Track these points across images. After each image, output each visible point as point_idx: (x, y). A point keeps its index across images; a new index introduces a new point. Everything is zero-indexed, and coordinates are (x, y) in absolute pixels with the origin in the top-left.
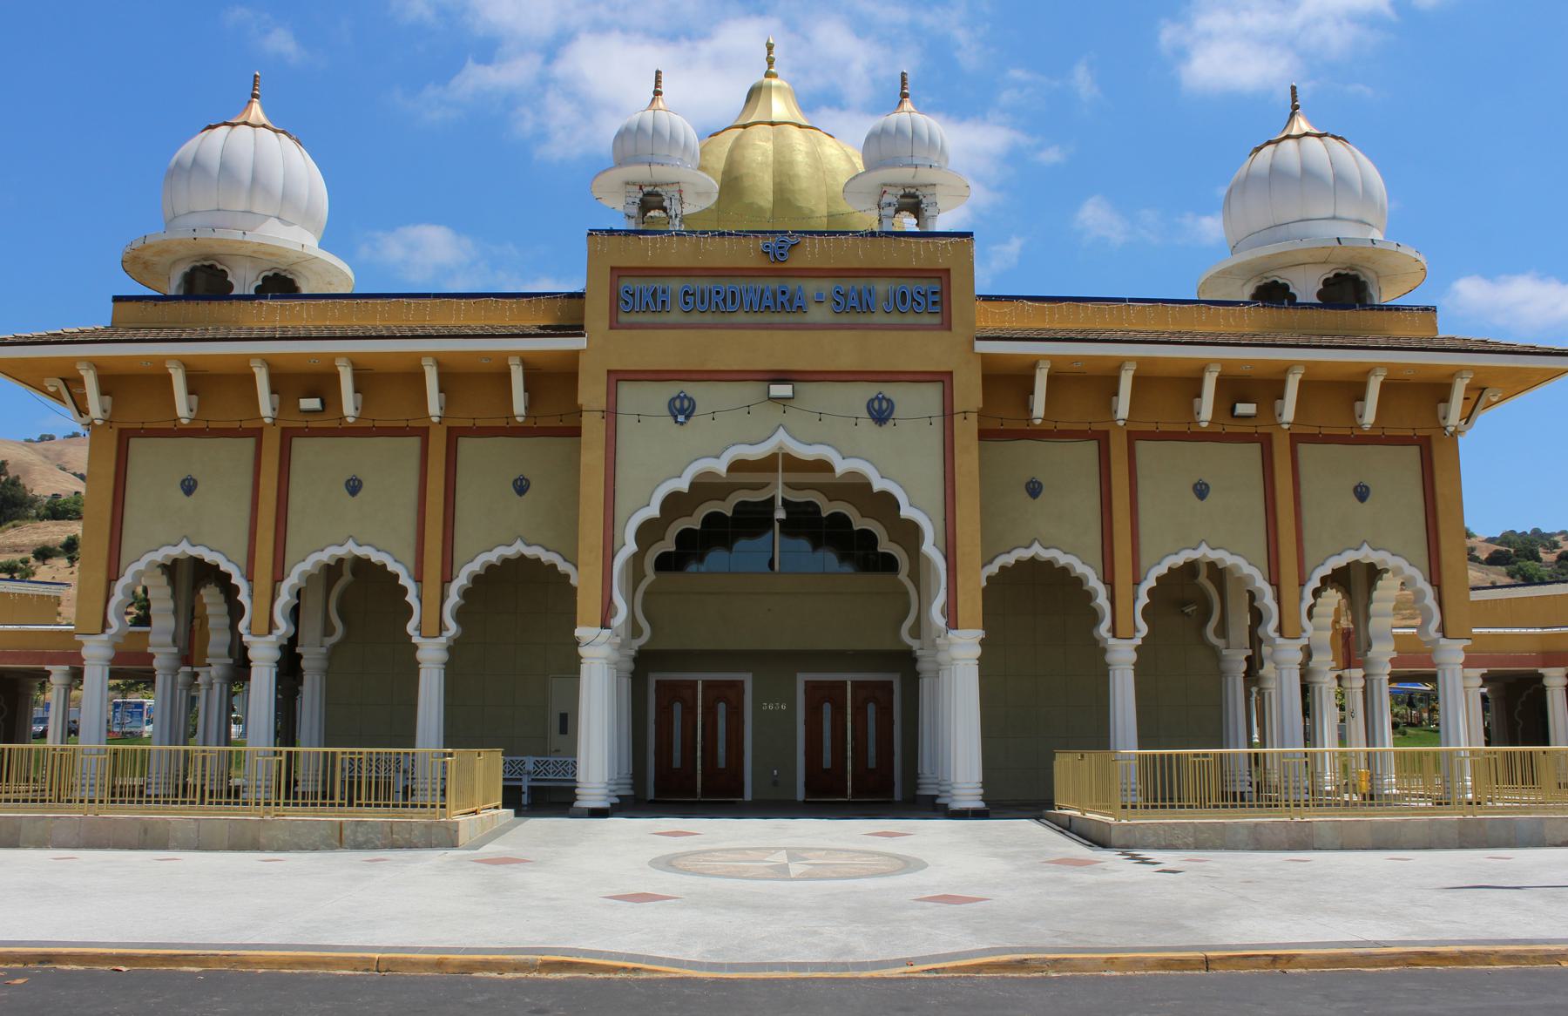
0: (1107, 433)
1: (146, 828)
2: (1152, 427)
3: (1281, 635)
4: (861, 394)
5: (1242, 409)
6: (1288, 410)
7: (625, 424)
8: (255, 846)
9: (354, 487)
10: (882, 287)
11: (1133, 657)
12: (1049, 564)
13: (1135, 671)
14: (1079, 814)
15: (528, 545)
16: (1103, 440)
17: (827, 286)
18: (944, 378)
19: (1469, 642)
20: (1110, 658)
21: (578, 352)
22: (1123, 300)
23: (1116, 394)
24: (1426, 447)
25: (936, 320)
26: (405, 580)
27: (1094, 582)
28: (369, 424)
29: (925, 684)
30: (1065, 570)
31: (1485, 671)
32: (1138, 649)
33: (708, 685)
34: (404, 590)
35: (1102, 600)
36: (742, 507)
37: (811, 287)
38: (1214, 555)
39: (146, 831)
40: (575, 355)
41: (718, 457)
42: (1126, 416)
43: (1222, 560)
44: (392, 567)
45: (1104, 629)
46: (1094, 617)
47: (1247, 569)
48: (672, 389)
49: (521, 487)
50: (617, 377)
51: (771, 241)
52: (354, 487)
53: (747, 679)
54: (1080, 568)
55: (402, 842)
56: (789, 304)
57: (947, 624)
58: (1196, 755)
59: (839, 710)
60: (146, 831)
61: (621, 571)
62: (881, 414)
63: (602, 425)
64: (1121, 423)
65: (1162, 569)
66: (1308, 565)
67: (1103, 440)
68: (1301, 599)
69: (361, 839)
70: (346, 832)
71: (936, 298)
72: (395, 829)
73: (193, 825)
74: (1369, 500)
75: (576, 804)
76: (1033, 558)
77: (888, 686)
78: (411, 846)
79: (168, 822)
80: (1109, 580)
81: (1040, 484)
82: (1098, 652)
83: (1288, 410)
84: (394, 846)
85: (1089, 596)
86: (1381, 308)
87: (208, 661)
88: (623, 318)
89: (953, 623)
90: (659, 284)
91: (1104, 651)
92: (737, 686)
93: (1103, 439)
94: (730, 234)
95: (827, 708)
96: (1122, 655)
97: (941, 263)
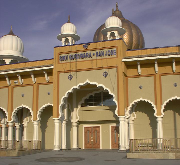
10: (105, 51)
12: (145, 101)
17: (95, 52)
18: (116, 67)
22: (158, 48)
26: (153, 105)
34: (153, 107)
36: (96, 94)
37: (92, 52)
40: (52, 69)
44: (150, 102)
45: (155, 114)
49: (49, 93)
50: (60, 72)
51: (85, 45)
61: (60, 108)
66: (163, 101)
75: (120, 150)
86: (176, 46)
87: (15, 126)
88: (60, 62)
92: (99, 127)
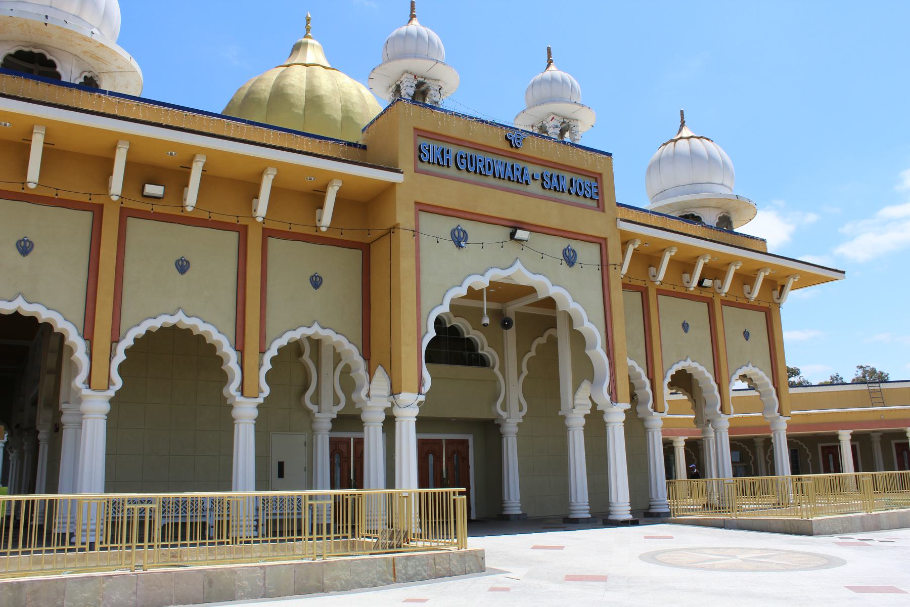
0: (101, 206)
1: (210, 579)
2: (286, 228)
3: (723, 412)
4: (558, 245)
5: (150, 189)
6: (262, 207)
7: (424, 241)
8: (320, 589)
9: (183, 267)
11: (255, 413)
13: (109, 428)
14: (865, 514)
15: (323, 328)
16: (243, 232)
19: (789, 418)
20: (235, 413)
21: (394, 184)
23: (257, 197)
24: (366, 249)
25: (594, 204)
27: (227, 349)
28: (205, 216)
29: (68, 435)
30: (201, 338)
31: (851, 431)
32: (112, 401)
33: (448, 442)
35: (232, 363)
37: (531, 169)
38: (309, 332)
39: (211, 583)
41: (483, 275)
42: (119, 192)
43: (196, 326)
45: (232, 388)
46: (224, 378)
47: (701, 368)
48: (453, 223)
50: (422, 208)
52: (183, 267)
53: (470, 439)
54: (60, 324)
55: (443, 572)
56: (518, 178)
57: (612, 400)
58: (134, 501)
59: (438, 459)
60: (211, 583)
62: (570, 259)
63: (413, 241)
64: (260, 220)
65: (140, 331)
67: (243, 232)
68: (260, 366)
69: (411, 572)
70: (399, 567)
71: (518, 174)
72: (437, 560)
73: (260, 573)
74: (321, 287)
76: (175, 326)
77: (465, 443)
78: (451, 574)
79: (233, 572)
80: (88, 335)
81: (32, 244)
82: (225, 410)
83: (262, 207)
84: (438, 576)
85: (220, 361)
89: (614, 399)
90: (446, 147)
91: (231, 407)
93: (97, 211)
94: (487, 122)
95: (431, 457)
96: (246, 411)
97: (598, 169)
